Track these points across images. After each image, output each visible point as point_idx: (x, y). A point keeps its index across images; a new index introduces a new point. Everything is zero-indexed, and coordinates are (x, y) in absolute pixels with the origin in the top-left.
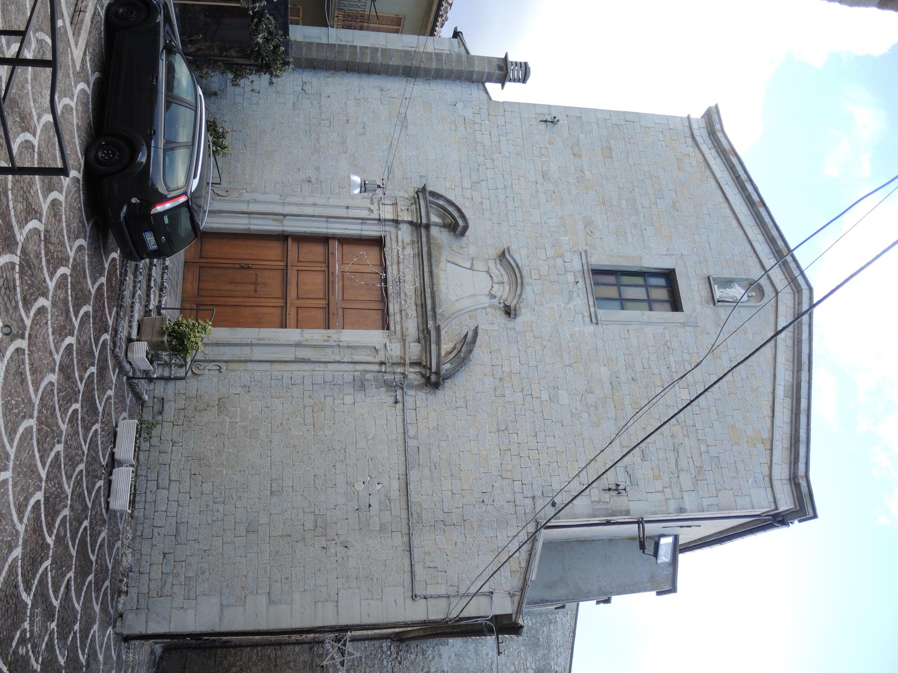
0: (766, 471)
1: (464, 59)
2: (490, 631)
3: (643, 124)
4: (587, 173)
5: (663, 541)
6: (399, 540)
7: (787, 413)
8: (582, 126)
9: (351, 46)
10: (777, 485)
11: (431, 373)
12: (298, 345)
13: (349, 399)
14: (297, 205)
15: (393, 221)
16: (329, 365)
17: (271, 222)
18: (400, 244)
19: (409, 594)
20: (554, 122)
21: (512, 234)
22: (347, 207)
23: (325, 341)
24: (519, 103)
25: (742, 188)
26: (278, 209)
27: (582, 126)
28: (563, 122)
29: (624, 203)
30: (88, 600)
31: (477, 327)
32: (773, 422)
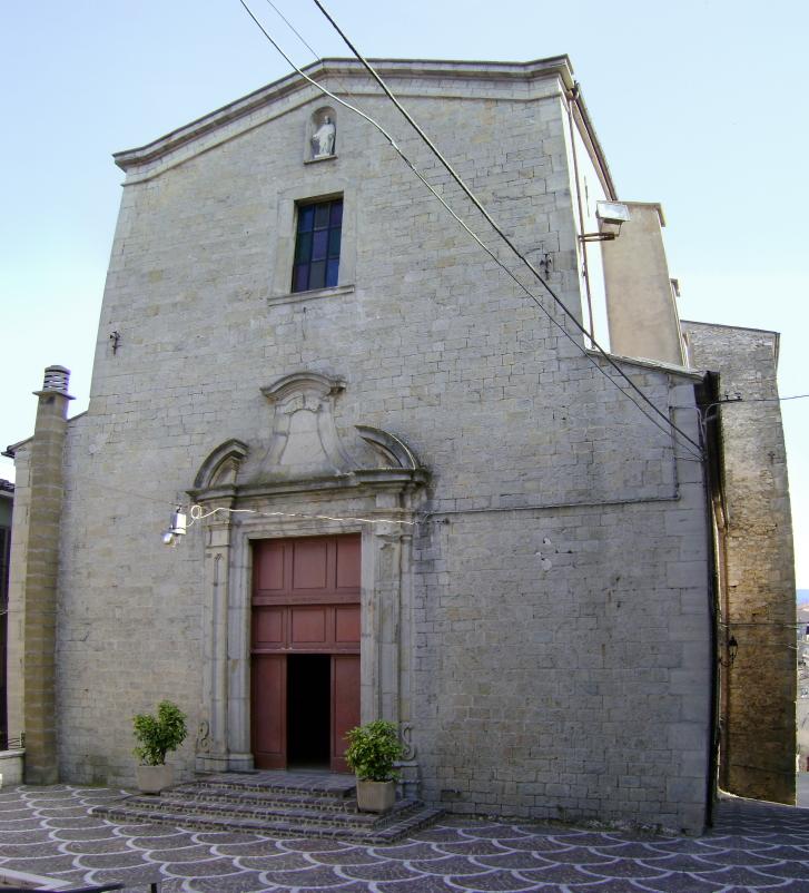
0: (522, 106)
1: (39, 443)
2: (715, 411)
3: (127, 235)
4: (178, 298)
5: (604, 214)
6: (610, 517)
7: (457, 84)
8: (124, 306)
9: (27, 584)
10: (534, 95)
11: (411, 482)
12: (379, 640)
13: (444, 579)
14: (214, 644)
15: (230, 530)
16: (403, 603)
17: (236, 674)
18: (257, 521)
19: (672, 506)
20: (116, 338)
21: (245, 386)
22: (216, 585)
23: (374, 608)
24: (93, 379)
25: (207, 130)
26: (220, 665)
27: (124, 306)
28: (116, 327)
29: (214, 257)
30: (662, 863)
31: (357, 427)
32: (466, 99)
